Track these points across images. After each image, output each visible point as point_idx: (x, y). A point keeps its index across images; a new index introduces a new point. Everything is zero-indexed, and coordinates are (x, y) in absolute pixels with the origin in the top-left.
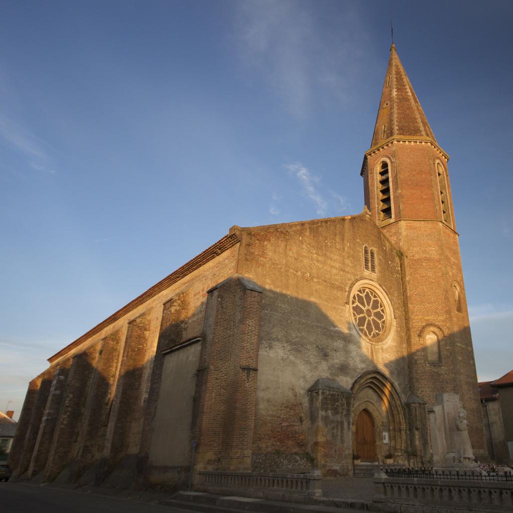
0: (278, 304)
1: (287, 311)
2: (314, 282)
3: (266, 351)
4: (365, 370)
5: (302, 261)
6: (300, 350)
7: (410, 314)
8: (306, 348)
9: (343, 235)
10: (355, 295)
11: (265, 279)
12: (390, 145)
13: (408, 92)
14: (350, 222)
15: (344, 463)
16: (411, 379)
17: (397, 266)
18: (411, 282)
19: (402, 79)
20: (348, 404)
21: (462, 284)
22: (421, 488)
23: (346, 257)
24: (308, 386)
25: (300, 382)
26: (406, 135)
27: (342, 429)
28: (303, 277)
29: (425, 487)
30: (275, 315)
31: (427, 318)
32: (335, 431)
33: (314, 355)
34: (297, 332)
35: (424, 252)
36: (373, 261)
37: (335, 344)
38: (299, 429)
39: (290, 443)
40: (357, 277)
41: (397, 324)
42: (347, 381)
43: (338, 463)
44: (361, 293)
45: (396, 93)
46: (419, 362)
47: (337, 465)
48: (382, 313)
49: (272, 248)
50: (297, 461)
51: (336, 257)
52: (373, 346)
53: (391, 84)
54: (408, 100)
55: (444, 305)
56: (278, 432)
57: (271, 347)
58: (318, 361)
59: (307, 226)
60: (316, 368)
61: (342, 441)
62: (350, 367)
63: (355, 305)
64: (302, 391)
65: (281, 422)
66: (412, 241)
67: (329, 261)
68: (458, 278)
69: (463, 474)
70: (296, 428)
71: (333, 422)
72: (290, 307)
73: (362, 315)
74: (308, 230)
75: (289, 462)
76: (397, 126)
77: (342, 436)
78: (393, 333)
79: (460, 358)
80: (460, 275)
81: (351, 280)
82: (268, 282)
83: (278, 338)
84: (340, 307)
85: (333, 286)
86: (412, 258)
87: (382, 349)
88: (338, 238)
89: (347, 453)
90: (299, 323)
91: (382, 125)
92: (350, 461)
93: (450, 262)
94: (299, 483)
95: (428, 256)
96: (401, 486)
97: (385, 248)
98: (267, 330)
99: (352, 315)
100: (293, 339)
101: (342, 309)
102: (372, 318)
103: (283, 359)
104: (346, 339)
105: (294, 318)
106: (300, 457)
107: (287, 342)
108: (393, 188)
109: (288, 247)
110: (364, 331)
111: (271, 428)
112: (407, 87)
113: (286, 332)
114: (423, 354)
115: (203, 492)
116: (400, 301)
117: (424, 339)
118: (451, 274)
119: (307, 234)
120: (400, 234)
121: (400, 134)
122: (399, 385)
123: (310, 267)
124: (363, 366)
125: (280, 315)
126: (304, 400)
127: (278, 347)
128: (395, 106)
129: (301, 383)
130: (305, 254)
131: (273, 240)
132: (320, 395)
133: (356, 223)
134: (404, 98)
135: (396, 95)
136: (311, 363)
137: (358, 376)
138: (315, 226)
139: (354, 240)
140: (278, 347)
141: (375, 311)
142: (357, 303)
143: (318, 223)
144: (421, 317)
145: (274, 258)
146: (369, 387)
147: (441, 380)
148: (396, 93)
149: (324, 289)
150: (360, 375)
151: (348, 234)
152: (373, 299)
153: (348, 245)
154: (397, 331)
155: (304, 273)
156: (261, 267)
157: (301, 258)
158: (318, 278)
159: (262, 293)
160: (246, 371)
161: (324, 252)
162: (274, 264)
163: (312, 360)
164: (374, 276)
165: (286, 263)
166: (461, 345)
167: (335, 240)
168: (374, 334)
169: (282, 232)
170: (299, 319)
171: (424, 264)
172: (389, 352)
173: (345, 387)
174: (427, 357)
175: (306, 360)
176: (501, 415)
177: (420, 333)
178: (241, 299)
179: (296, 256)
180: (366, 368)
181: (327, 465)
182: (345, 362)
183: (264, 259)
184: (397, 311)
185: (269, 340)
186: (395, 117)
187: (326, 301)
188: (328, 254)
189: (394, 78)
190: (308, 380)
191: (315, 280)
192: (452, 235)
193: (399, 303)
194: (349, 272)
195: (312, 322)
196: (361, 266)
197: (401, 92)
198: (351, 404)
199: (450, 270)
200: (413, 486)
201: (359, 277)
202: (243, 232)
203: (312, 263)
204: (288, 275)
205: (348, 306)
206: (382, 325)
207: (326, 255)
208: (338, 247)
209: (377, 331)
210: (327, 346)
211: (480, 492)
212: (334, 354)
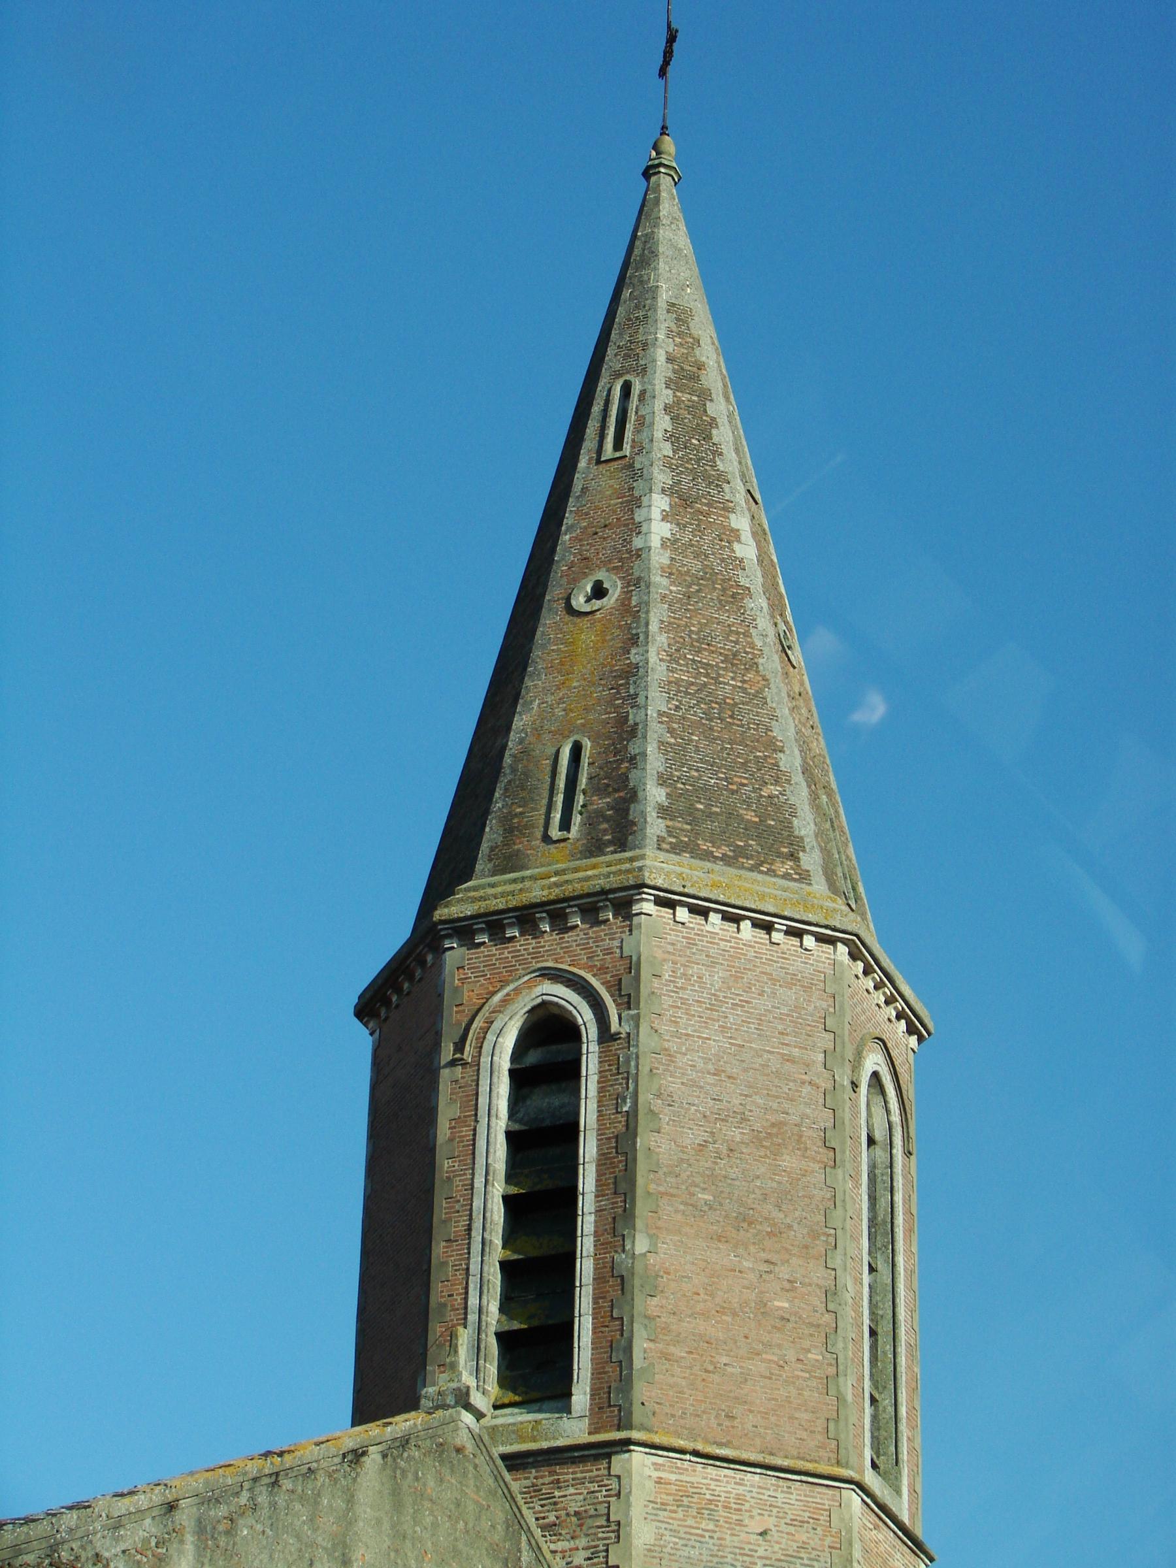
13: (736, 535)
19: (705, 429)
26: (708, 856)
53: (639, 448)
54: (735, 596)
59: (186, 1516)
76: (663, 780)
108: (599, 1211)
112: (737, 492)
120: (618, 1530)
134: (709, 576)
135: (664, 543)
189: (658, 405)
197: (699, 531)
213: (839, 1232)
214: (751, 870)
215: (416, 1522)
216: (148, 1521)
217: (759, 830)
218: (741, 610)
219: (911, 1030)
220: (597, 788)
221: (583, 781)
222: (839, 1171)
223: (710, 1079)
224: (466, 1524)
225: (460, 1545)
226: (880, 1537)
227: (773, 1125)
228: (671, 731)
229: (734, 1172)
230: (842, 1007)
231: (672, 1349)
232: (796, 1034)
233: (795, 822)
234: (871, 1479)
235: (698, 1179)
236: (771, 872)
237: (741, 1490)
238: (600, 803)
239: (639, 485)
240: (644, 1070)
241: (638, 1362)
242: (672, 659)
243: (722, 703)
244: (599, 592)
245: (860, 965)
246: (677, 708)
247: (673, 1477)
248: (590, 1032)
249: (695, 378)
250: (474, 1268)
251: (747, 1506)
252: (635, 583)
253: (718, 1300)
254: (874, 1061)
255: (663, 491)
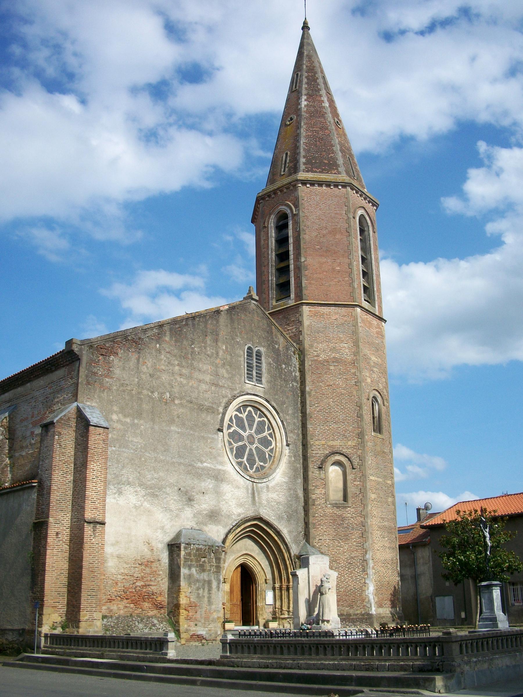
0: (128, 438)
1: (140, 446)
2: (176, 405)
3: (115, 498)
4: (242, 516)
5: (159, 378)
6: (157, 496)
7: (309, 438)
8: (164, 492)
9: (217, 335)
10: (232, 416)
11: (112, 406)
12: (292, 188)
13: (323, 101)
14: (228, 313)
15: (211, 628)
16: (307, 524)
17: (294, 370)
18: (313, 393)
20: (218, 560)
21: (385, 393)
22: (259, 646)
23: (220, 365)
24: (168, 539)
25: (157, 534)
26: (316, 172)
27: (210, 589)
28: (161, 399)
29: (263, 645)
30: (125, 452)
31: (331, 443)
32: (201, 591)
33: (175, 500)
34: (153, 472)
35: (333, 350)
36: (259, 368)
37: (203, 484)
38: (157, 589)
39: (146, 605)
40: (236, 392)
41: (289, 453)
42: (218, 531)
43: (205, 628)
44: (241, 413)
45: (306, 103)
46: (318, 502)
47: (202, 629)
48: (269, 438)
49: (121, 364)
50: (154, 625)
51: (205, 367)
52: (255, 484)
55: (356, 425)
56: (130, 592)
57: (120, 493)
58: (180, 507)
59: (166, 328)
60: (177, 516)
61: (210, 603)
62: (223, 513)
63: (231, 431)
64: (160, 545)
65: (135, 581)
66: (317, 335)
67: (196, 375)
68: (380, 385)
69: (318, 635)
70: (153, 588)
71: (198, 581)
72: (144, 441)
73: (240, 443)
74: (168, 333)
75: (145, 626)
76: (304, 157)
77: (209, 598)
78: (284, 465)
79: (373, 496)
80: (384, 380)
81: (226, 396)
82: (115, 410)
83: (129, 482)
84: (210, 435)
85: (201, 408)
86: (316, 358)
87: (268, 487)
88: (209, 339)
89: (216, 617)
90: (156, 460)
91: (283, 152)
92: (220, 625)
93: (368, 363)
94: (153, 645)
95: (337, 356)
96: (244, 645)
97: (277, 346)
98: (115, 472)
99: (227, 444)
100: (149, 481)
101: (213, 438)
102: (255, 446)
103: (136, 507)
104: (217, 478)
105: (148, 455)
106: (158, 621)
107: (140, 485)
109: (141, 360)
110: (243, 465)
111: (123, 589)
113: (139, 473)
114: (323, 492)
115: (56, 655)
116: (296, 421)
117: (326, 472)
118: (369, 380)
119: (167, 338)
121: (307, 171)
122: (290, 532)
123: (169, 384)
124: (240, 510)
125: (132, 451)
126: (162, 556)
127: (129, 493)
128: (302, 124)
129: (159, 535)
130: (163, 367)
131: (121, 352)
132: (182, 549)
133: (236, 316)
134: (317, 111)
136: (171, 511)
137: (234, 524)
138: (177, 326)
139: (233, 339)
140: (129, 493)
141: (260, 436)
142: (235, 428)
143: (182, 320)
144: (323, 442)
145: (123, 377)
146: (249, 537)
147: (345, 525)
148: (306, 103)
149: (188, 413)
150: (236, 522)
151: (224, 332)
152: (257, 419)
153: (224, 348)
154: (290, 462)
155: (162, 394)
156: (106, 391)
157: (158, 373)
158: (181, 399)
159: (108, 429)
160: (92, 525)
161: (190, 362)
162: (122, 385)
163: (173, 507)
164: (260, 389)
165: (138, 383)
166: (376, 479)
167: (206, 343)
168: (257, 468)
169: (133, 341)
170: (156, 455)
171: (332, 368)
172: (276, 491)
173: (216, 539)
174: (328, 495)
175: (166, 506)
176: (431, 563)
177: (322, 464)
178: (82, 437)
179: (151, 372)
180: (244, 513)
181: (190, 630)
182: (215, 506)
183: (109, 380)
184: (291, 435)
185: (118, 484)
186: (302, 143)
187: (191, 429)
188: (195, 363)
189: (304, 77)
190: (168, 531)
191: (177, 402)
192: (375, 322)
193: (294, 424)
194: (224, 387)
195: (172, 458)
196: (241, 376)
198: (222, 560)
199: (368, 375)
200: (253, 645)
201: (238, 391)
202: (83, 347)
203: (172, 378)
204: (141, 399)
205: (222, 433)
206: (269, 454)
207: (192, 365)
208: (209, 352)
209: (262, 464)
210: (193, 488)
211: (303, 647)
212: (201, 498)
213: (351, 251)
214: (326, 173)
215: (238, 324)
216: (154, 330)
217: (329, 164)
218: (324, 117)
219: (373, 205)
220: (291, 161)
221: (288, 161)
222: (351, 237)
223: (317, 221)
224: (255, 324)
225: (253, 329)
226: (368, 317)
227: (334, 229)
228: (307, 146)
229: (325, 241)
230: (349, 200)
231: (312, 282)
232: (338, 208)
233: (337, 161)
234: (365, 304)
235: (316, 243)
236: (331, 173)
237: (330, 310)
238: (291, 165)
239: (300, 94)
240: (301, 220)
241: (303, 285)
242: (307, 130)
243: (319, 138)
244: (291, 119)
245: (354, 192)
246: (308, 141)
247: (313, 310)
248: (290, 215)
249: (313, 69)
250: (270, 271)
251: (332, 314)
252: (299, 115)
253: (322, 269)
254: (360, 212)
255: (305, 95)
